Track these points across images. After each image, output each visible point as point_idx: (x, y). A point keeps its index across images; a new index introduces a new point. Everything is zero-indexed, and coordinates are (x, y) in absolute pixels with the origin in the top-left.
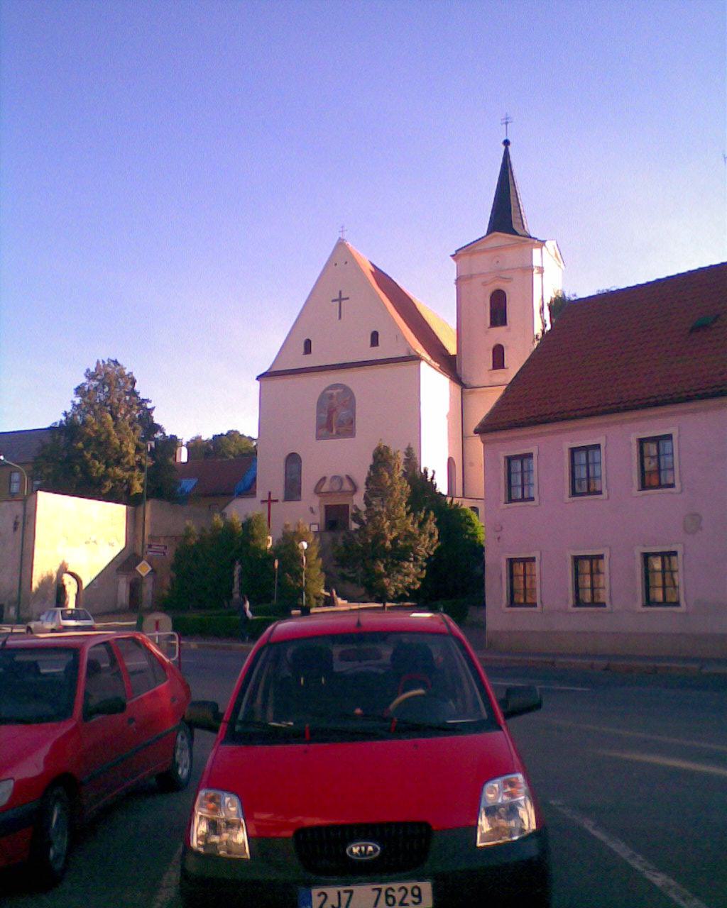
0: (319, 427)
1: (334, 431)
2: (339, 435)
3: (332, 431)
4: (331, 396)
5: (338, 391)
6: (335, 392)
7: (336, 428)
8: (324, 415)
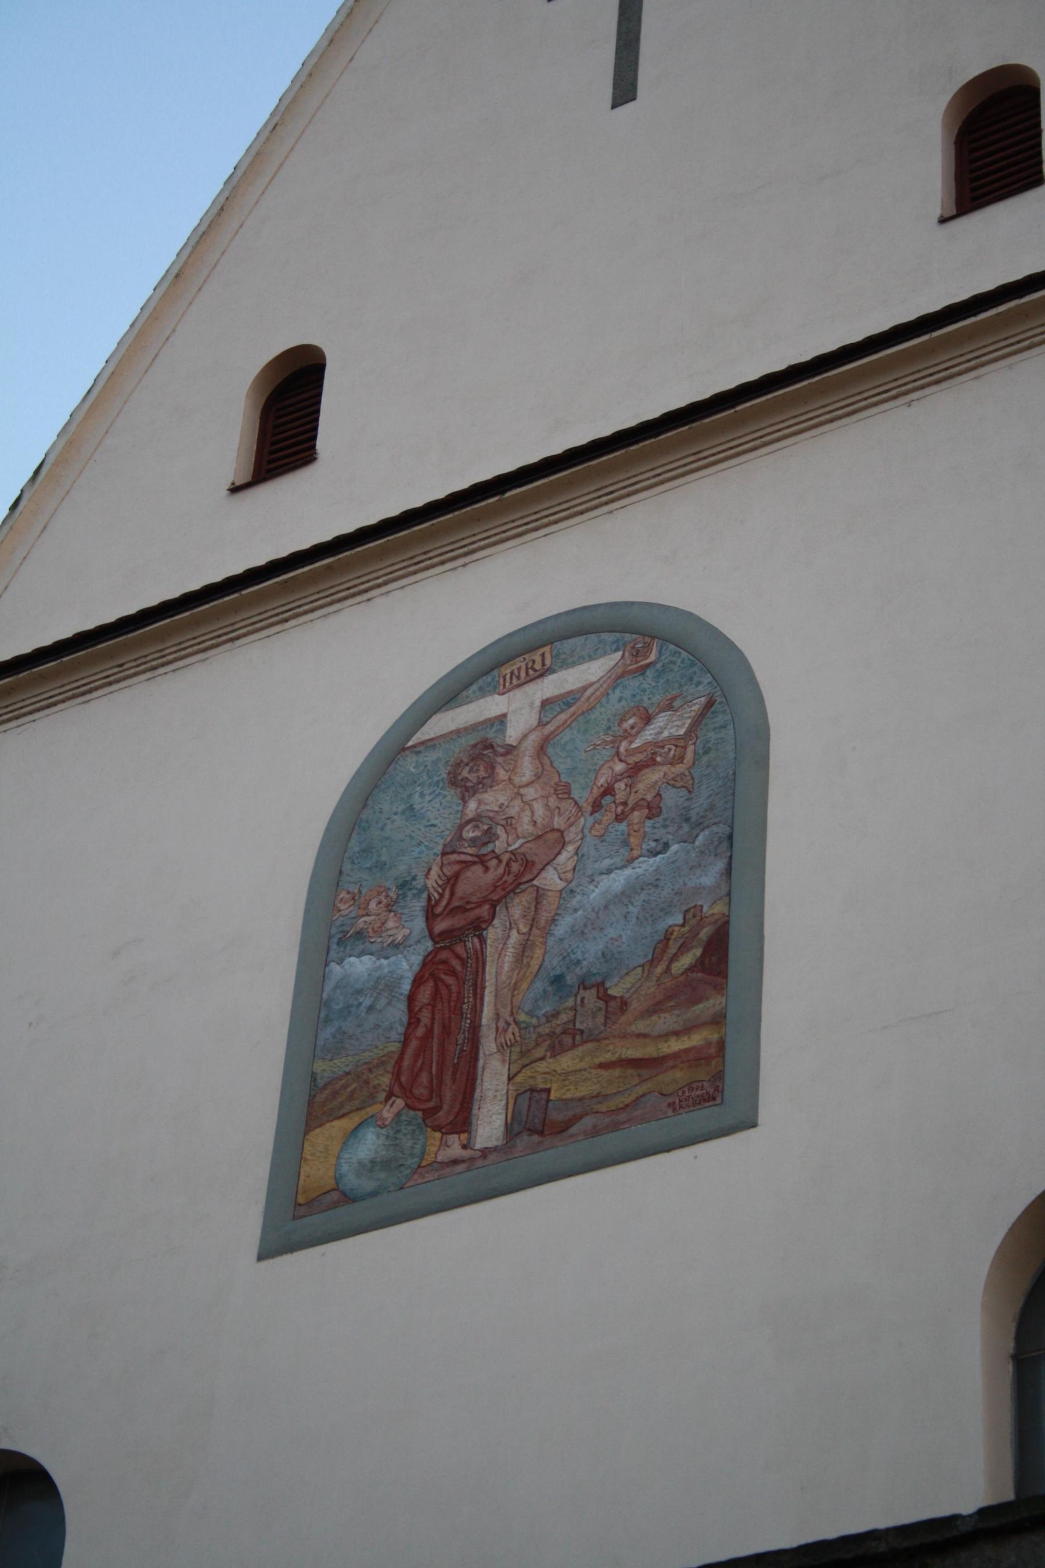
0: (316, 1100)
1: (490, 1124)
2: (552, 1137)
3: (462, 1123)
4: (483, 755)
5: (550, 686)
6: (518, 710)
7: (521, 1054)
8: (390, 965)
